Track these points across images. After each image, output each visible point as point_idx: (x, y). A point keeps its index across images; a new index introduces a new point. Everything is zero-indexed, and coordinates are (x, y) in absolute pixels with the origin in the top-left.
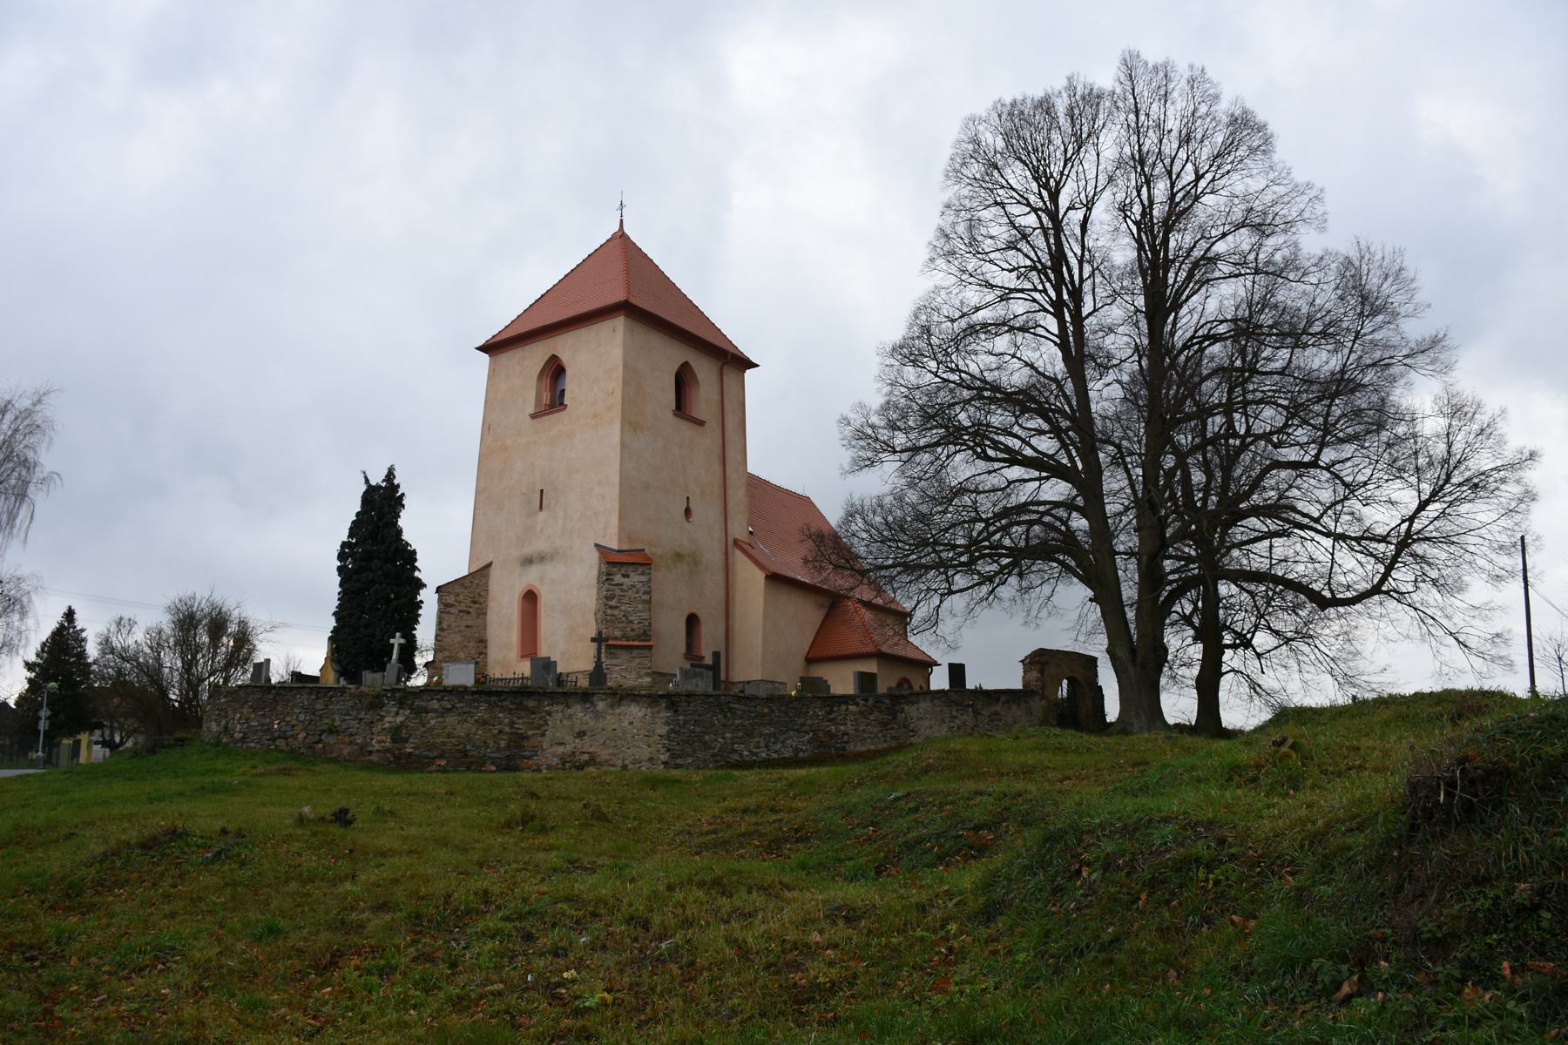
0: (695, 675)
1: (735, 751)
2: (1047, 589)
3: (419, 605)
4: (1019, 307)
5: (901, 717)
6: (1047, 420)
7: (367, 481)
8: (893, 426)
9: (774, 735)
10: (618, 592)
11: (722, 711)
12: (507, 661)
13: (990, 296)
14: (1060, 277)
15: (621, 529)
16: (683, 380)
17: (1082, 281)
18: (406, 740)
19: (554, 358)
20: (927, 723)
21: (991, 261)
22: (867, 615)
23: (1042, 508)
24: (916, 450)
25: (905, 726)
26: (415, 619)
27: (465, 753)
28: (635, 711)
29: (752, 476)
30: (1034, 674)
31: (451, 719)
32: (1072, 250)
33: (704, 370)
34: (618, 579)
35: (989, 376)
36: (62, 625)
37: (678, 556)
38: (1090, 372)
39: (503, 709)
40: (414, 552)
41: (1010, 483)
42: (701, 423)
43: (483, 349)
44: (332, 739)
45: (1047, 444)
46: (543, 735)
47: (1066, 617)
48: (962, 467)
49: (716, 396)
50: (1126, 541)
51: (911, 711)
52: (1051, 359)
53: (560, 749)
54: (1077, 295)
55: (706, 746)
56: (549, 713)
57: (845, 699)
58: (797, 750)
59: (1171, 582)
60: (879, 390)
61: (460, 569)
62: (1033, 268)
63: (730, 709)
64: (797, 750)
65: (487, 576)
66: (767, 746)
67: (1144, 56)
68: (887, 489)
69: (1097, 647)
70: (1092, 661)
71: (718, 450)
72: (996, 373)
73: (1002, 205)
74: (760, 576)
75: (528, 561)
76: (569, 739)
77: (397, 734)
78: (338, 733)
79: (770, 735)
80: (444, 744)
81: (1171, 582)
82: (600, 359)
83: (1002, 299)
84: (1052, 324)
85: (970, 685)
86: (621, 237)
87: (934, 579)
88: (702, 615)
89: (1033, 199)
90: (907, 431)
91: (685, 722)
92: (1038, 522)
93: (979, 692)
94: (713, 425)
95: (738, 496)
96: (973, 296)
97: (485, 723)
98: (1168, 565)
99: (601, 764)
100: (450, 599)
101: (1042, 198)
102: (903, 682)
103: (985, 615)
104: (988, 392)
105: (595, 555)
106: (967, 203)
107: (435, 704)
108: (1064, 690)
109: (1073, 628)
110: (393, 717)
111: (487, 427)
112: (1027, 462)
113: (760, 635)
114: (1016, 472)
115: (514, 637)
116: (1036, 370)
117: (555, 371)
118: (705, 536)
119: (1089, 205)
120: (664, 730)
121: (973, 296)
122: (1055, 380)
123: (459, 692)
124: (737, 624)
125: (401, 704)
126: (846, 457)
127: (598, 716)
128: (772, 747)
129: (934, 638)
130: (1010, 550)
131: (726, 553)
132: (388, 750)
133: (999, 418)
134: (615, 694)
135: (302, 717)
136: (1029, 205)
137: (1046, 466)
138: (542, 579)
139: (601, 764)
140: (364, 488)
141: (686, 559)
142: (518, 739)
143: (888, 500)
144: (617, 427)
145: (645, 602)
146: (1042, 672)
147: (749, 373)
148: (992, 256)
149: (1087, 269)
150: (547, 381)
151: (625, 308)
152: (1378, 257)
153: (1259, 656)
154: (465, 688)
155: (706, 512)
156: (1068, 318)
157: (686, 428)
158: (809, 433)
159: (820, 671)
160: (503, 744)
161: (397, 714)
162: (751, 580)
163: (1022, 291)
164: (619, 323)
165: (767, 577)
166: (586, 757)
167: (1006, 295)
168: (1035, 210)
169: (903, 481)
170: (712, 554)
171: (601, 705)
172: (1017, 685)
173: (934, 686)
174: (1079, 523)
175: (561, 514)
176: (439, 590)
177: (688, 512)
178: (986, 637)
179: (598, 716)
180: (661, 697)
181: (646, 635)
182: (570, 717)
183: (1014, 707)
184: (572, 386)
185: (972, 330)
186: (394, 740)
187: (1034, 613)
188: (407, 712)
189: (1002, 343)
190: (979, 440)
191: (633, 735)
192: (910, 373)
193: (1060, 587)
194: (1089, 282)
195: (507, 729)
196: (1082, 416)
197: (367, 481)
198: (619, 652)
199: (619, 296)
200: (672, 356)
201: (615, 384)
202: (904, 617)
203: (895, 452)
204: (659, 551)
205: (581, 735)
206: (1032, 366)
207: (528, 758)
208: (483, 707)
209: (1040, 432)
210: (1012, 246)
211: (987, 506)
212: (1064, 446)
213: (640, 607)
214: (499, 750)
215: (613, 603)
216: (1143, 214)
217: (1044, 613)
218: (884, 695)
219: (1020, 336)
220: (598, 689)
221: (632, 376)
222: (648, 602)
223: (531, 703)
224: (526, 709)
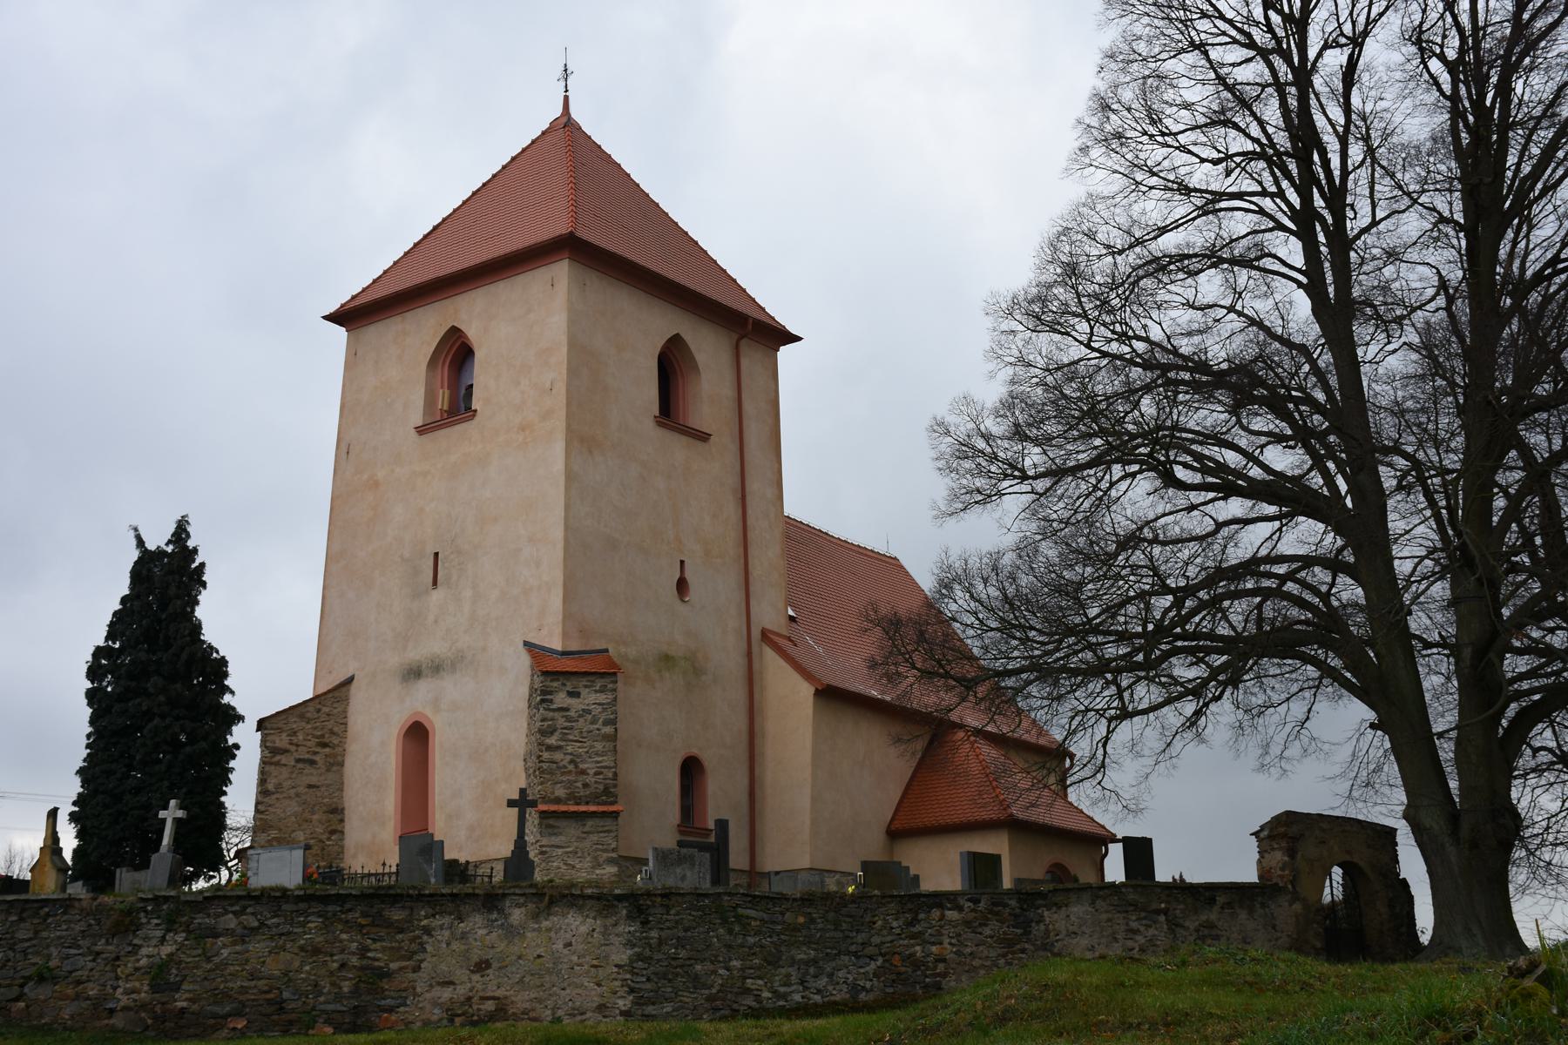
0: (681, 860)
1: (748, 991)
2: (1298, 708)
3: (231, 752)
4: (1239, 224)
5: (1037, 930)
6: (1285, 416)
7: (140, 542)
8: (1018, 434)
9: (815, 961)
10: (561, 722)
11: (725, 921)
12: (372, 843)
13: (1182, 209)
14: (1306, 171)
15: (567, 616)
16: (672, 366)
17: (1345, 173)
18: (177, 987)
19: (455, 334)
20: (1084, 942)
21: (1183, 149)
22: (988, 752)
23: (1281, 569)
24: (1057, 473)
26: (223, 777)
27: (280, 1005)
28: (576, 924)
29: (792, 523)
30: (1278, 857)
31: (258, 947)
32: (1327, 117)
34: (561, 699)
35: (1186, 346)
37: (667, 660)
38: (1361, 331)
39: (349, 926)
40: (223, 662)
41: (1219, 526)
42: (703, 437)
43: (336, 318)
44: (43, 992)
45: (1283, 460)
46: (417, 969)
47: (1324, 755)
48: (1137, 498)
49: (728, 391)
50: (1429, 618)
52: (1298, 312)
53: (446, 994)
54: (1337, 197)
55: (697, 982)
57: (940, 899)
58: (855, 989)
59: (1518, 695)
60: (992, 375)
61: (300, 688)
62: (1261, 156)
63: (739, 918)
64: (855, 989)
65: (345, 700)
66: (802, 982)
68: (1010, 540)
69: (1387, 806)
70: (1387, 836)
71: (732, 480)
72: (1196, 339)
73: (1201, 48)
74: (806, 691)
75: (414, 673)
76: (461, 974)
77: (161, 977)
78: (55, 980)
79: (807, 963)
81: (1518, 695)
82: (529, 332)
83: (1204, 211)
84: (1292, 251)
85: (1163, 874)
86: (565, 129)
87: (1099, 694)
88: (708, 759)
89: (1259, 36)
90: (1044, 441)
91: (661, 942)
92: (1278, 593)
93: (1179, 888)
94: (723, 439)
95: (768, 556)
96: (1154, 208)
97: (316, 951)
98: (1515, 664)
100: (281, 741)
101: (1270, 30)
102: (1059, 872)
103: (1188, 750)
104: (1174, 371)
105: (525, 660)
106: (1142, 47)
107: (230, 921)
108: (1334, 887)
109: (1343, 775)
110: (156, 946)
111: (345, 449)
112: (1255, 491)
113: (807, 791)
114: (1236, 507)
115: (390, 802)
116: (1268, 331)
117: (456, 354)
118: (712, 624)
119: (1357, 41)
120: (622, 956)
121: (1154, 208)
122: (1303, 349)
123: (275, 898)
124: (771, 773)
125: (170, 924)
126: (939, 487)
127: (512, 933)
128: (812, 984)
129: (1098, 793)
130: (1219, 641)
131: (749, 654)
132: (143, 1006)
133: (1208, 416)
134: (540, 895)
136: (1251, 44)
137: (1288, 497)
138: (436, 703)
140: (135, 555)
142: (374, 977)
143: (1008, 559)
144: (559, 447)
145: (606, 737)
146: (1291, 853)
147: (785, 353)
148: (1182, 139)
149: (1356, 152)
150: (443, 372)
154: (284, 891)
155: (714, 588)
156: (1322, 238)
157: (678, 447)
158: (880, 447)
160: (346, 987)
161: (163, 940)
162: (790, 698)
163: (1239, 196)
164: (561, 271)
165: (818, 693)
166: (490, 1006)
167: (1212, 203)
168: (1264, 53)
169: (1034, 526)
170: (725, 654)
171: (517, 915)
172: (1248, 873)
173: (1109, 878)
174: (1349, 591)
176: (262, 724)
177: (682, 586)
178: (1198, 790)
179: (512, 933)
180: (620, 898)
181: (608, 793)
182: (464, 936)
183: (1243, 915)
185: (1159, 266)
186: (155, 988)
187: (1275, 750)
188: (180, 937)
189: (1211, 285)
190: (1157, 451)
191: (571, 962)
192: (1045, 341)
193: (1322, 706)
194: (1364, 173)
195: (354, 961)
196: (1350, 404)
197: (140, 542)
198: (562, 823)
199: (558, 227)
200: (646, 327)
201: (555, 373)
202: (1055, 758)
203: (1024, 477)
204: (632, 652)
205: (482, 966)
206: (1259, 324)
207: (391, 1010)
208: (314, 923)
209: (1278, 438)
210: (1220, 120)
211: (1185, 565)
212: (1318, 464)
213: (599, 746)
214: (339, 997)
215: (552, 741)
216: (1462, 51)
217: (1294, 750)
218: (1008, 893)
219: (1243, 275)
220: (517, 886)
222: (613, 738)
223: (397, 915)
224: (389, 924)
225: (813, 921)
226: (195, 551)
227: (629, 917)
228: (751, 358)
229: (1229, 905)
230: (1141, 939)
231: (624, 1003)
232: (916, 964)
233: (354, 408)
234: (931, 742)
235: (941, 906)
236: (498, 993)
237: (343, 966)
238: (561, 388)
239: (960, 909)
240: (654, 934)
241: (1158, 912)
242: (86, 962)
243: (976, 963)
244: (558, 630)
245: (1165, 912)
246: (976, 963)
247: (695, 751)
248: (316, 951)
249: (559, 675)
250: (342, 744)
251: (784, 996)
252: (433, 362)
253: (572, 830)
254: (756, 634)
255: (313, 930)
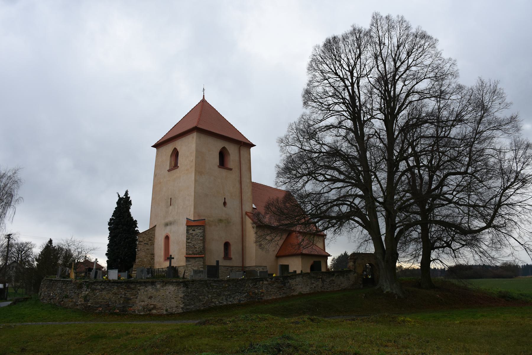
5: (287, 285)
7: (119, 196)
9: (229, 295)
11: (207, 286)
15: (194, 212)
16: (223, 155)
18: (88, 301)
20: (300, 286)
25: (289, 288)
27: (108, 305)
31: (104, 293)
33: (232, 149)
34: (191, 232)
36: (47, 245)
37: (221, 221)
42: (231, 169)
43: (156, 146)
46: (137, 298)
49: (237, 158)
51: (292, 282)
53: (143, 303)
55: (200, 300)
56: (139, 290)
58: (240, 301)
61: (147, 228)
64: (240, 301)
65: (154, 230)
67: (381, 14)
71: (238, 179)
75: (167, 225)
76: (146, 299)
79: (228, 295)
80: (101, 302)
86: (203, 102)
88: (231, 242)
91: (191, 292)
97: (116, 294)
99: (158, 309)
107: (99, 287)
111: (155, 175)
115: (162, 253)
117: (175, 154)
120: (182, 295)
127: (157, 290)
131: (242, 218)
132: (82, 304)
135: (59, 291)
139: (158, 309)
141: (225, 222)
142: (127, 300)
146: (354, 262)
150: (174, 158)
151: (196, 129)
152: (488, 84)
153: (454, 250)
157: (224, 172)
159: (284, 261)
160: (122, 302)
164: (195, 135)
166: (152, 306)
170: (236, 218)
171: (158, 286)
175: (176, 207)
177: (225, 204)
179: (157, 290)
182: (147, 291)
183: (341, 278)
184: (181, 160)
186: (85, 301)
188: (89, 290)
195: (123, 296)
197: (119, 196)
198: (191, 259)
199: (194, 125)
200: (217, 146)
201: (193, 158)
205: (150, 298)
207: (131, 307)
208: (115, 288)
213: (199, 242)
214: (120, 304)
215: (189, 241)
221: (200, 155)
223: (132, 286)
224: (131, 288)
225: (230, 285)
226: (129, 197)
227: (183, 286)
228: (243, 151)
229: (338, 275)
230: (314, 285)
231: (182, 306)
232: (256, 294)
233: (157, 166)
234: (288, 235)
235: (263, 281)
236: (154, 303)
237: (121, 297)
238: (194, 161)
239: (268, 281)
240: (190, 290)
241: (319, 278)
242: (73, 294)
243: (271, 293)
244: (193, 216)
245: (321, 278)
246: (271, 293)
247: (228, 241)
248: (116, 294)
249: (190, 226)
250: (154, 240)
251: (222, 303)
252: (171, 156)
253: (193, 261)
254: (244, 213)
255: (115, 289)
